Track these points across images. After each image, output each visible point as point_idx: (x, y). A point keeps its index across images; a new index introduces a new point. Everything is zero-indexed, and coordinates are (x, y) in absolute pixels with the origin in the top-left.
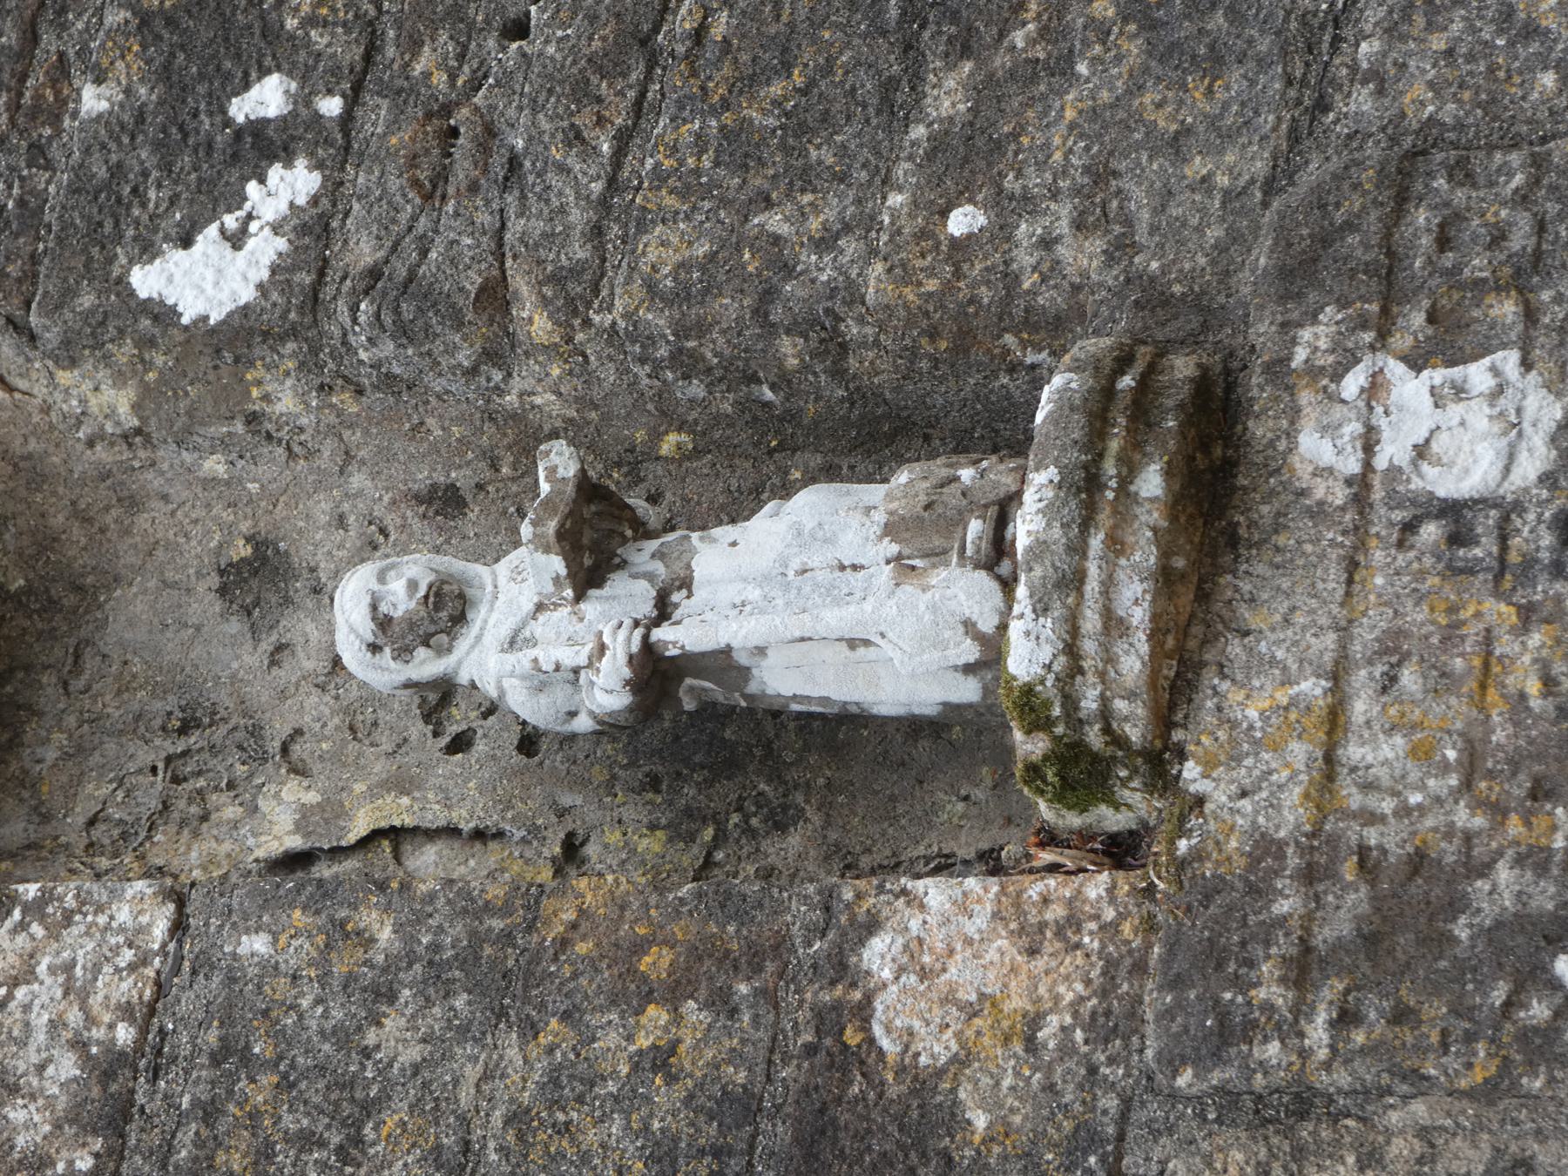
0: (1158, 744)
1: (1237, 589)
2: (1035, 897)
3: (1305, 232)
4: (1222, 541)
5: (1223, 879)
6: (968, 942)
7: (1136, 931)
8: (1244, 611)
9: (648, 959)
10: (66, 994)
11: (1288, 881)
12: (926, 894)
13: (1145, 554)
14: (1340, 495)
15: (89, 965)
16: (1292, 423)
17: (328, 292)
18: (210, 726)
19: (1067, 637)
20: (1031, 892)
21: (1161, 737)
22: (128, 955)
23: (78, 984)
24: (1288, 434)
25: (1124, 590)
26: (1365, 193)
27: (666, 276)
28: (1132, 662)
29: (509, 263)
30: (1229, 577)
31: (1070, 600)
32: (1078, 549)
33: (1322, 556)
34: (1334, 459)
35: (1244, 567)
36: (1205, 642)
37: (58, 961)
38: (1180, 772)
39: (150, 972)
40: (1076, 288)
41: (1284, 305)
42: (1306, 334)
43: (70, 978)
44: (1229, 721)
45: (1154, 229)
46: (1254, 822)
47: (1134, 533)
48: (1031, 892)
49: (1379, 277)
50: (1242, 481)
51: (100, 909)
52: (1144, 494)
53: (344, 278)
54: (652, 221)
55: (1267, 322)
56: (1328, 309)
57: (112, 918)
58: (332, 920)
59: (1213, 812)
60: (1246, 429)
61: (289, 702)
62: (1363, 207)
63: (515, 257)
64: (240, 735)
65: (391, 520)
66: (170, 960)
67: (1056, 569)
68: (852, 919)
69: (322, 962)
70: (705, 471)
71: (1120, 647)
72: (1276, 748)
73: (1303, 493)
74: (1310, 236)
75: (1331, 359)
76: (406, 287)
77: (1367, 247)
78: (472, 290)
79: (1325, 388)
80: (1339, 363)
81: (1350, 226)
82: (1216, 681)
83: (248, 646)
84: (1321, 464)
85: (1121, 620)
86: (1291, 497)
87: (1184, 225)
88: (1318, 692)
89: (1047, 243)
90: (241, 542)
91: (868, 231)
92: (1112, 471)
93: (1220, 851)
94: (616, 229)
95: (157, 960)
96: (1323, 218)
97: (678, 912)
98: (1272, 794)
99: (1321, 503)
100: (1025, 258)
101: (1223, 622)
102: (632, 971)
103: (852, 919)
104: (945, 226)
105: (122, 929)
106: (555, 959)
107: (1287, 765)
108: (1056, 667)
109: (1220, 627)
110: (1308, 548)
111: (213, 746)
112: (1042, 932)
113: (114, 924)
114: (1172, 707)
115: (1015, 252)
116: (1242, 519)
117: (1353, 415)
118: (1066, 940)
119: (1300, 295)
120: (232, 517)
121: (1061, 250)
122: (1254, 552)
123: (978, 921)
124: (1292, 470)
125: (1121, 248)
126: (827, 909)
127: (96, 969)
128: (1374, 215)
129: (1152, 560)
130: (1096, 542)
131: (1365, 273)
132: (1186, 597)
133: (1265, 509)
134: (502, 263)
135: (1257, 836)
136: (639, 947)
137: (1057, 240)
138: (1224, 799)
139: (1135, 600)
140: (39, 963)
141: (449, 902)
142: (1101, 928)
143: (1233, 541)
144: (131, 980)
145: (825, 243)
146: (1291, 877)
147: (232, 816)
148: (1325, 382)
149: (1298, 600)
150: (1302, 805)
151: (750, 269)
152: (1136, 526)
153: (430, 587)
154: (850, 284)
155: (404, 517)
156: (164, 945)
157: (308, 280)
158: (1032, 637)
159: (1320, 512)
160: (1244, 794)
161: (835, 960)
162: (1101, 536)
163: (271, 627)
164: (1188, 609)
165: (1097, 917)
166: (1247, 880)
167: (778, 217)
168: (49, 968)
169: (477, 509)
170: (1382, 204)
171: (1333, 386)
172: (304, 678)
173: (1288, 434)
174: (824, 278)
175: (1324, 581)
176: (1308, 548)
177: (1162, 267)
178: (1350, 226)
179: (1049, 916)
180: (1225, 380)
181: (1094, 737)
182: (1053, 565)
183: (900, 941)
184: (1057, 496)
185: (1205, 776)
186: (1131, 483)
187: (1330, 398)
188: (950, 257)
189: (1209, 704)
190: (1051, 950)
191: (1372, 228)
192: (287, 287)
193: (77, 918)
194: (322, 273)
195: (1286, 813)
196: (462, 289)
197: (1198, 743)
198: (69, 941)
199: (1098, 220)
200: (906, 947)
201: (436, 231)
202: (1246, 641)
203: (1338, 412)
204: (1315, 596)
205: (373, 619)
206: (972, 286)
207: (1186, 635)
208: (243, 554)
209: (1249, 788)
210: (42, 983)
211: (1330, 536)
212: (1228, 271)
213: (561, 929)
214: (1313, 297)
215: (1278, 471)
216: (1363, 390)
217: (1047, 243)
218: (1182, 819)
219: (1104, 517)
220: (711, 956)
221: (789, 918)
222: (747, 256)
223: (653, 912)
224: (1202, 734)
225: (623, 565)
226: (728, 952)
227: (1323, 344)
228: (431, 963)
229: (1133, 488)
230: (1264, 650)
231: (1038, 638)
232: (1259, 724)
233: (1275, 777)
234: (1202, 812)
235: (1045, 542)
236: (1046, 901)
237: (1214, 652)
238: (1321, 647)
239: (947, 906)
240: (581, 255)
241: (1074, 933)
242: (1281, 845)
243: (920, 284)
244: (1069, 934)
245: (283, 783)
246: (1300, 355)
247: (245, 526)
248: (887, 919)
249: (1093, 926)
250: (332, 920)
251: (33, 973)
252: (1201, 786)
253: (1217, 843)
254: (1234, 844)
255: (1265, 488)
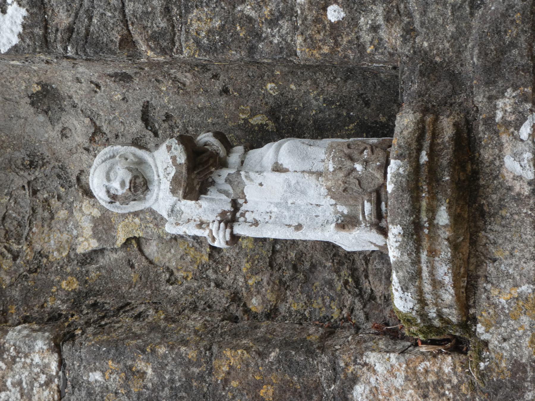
0: (464, 319)
1: (487, 238)
2: (422, 370)
3: (493, 48)
4: (477, 214)
5: (502, 382)
6: (397, 390)
7: (467, 389)
8: (491, 248)
9: (262, 391)
10: (22, 396)
11: (529, 384)
12: (375, 365)
13: (445, 252)
14: (526, 189)
15: (28, 382)
16: (500, 151)
17: (52, 37)
18: (43, 166)
19: (419, 298)
20: (420, 368)
21: (465, 315)
22: (43, 378)
23: (26, 391)
24: (499, 157)
25: (439, 270)
26: (517, 26)
27: (204, 37)
28: (448, 296)
29: (131, 27)
30: (483, 232)
31: (417, 284)
32: (417, 262)
33: (523, 222)
34: (521, 171)
35: (489, 227)
36: (477, 266)
37: (15, 381)
38: (476, 329)
39: (54, 386)
40: (391, 55)
41: (488, 87)
42: (500, 103)
43: (22, 389)
44: (493, 304)
45: (422, 24)
46: (511, 355)
47: (439, 245)
48: (420, 368)
49: (529, 72)
50: (482, 182)
51: (26, 356)
52: (441, 223)
53: (57, 30)
54: (192, 7)
55: (482, 96)
56: (508, 90)
57: (32, 360)
58: (126, 366)
59: (493, 349)
60: (480, 155)
61: (75, 156)
62: (518, 33)
63: (133, 24)
64: (57, 170)
65: (101, 82)
66: (61, 380)
67: (408, 273)
68: (346, 376)
69: (126, 386)
70: (237, 68)
71: (442, 292)
72: (516, 318)
73: (510, 189)
74: (495, 49)
75: (513, 117)
76: (86, 39)
77: (522, 57)
78: (117, 41)
79: (513, 133)
80: (518, 119)
81: (513, 45)
82: (485, 285)
83: (50, 127)
84: (516, 174)
85: (440, 282)
86: (505, 191)
87: (436, 23)
88: (530, 291)
89: (375, 28)
90: (35, 86)
91: (291, 17)
92: (425, 219)
93: (498, 367)
94: (175, 10)
95: (56, 380)
96: (500, 40)
97: (272, 369)
98: (517, 340)
99: (519, 194)
100: (366, 37)
101: (484, 256)
102: (257, 396)
103: (346, 376)
104: (326, 15)
105: (38, 365)
106: (224, 389)
107: (522, 327)
108: (415, 308)
109: (483, 258)
110: (516, 217)
111: (47, 176)
112: (428, 388)
113: (34, 363)
114: (468, 298)
115: (361, 34)
116: (484, 202)
117: (527, 149)
118: (438, 392)
119: (495, 82)
120: (28, 76)
121: (382, 33)
122: (492, 219)
123: (400, 380)
124: (503, 177)
125: (409, 32)
126: (334, 369)
127: (31, 384)
128: (523, 38)
129: (449, 254)
130: (424, 256)
131: (523, 71)
132: (465, 248)
133: (494, 197)
134: (127, 26)
135: (513, 361)
136: (258, 386)
137: (379, 27)
138: (496, 342)
139: (444, 272)
140: (6, 381)
141: (173, 359)
142: (452, 387)
143: (483, 214)
144: (47, 391)
145: (273, 22)
146: (530, 382)
147: (63, 216)
148: (512, 130)
149: (516, 244)
150: (530, 346)
151: (241, 35)
152: (440, 241)
153: (130, 183)
154: (288, 45)
155: (105, 82)
156: (57, 373)
157: (41, 33)
158: (404, 299)
159: (518, 199)
160: (505, 340)
161: (342, 396)
162: (425, 253)
163: (58, 120)
164: (468, 251)
165: (450, 381)
166: (512, 383)
167: (249, 7)
168: (12, 384)
169: (137, 79)
170: (526, 31)
171: (516, 132)
172: (79, 145)
173: (499, 157)
174: (276, 41)
175: (525, 234)
176: (516, 217)
177: (429, 46)
178: (513, 45)
179: (429, 380)
180: (467, 128)
181: (437, 323)
182: (407, 271)
183: (368, 388)
184: (403, 240)
185: (487, 332)
186: (434, 219)
187: (515, 138)
188: (331, 34)
189: (483, 296)
190: (433, 396)
191: (524, 46)
192: (32, 36)
193: (18, 359)
194: (46, 28)
195: (524, 350)
196: (112, 41)
197: (481, 315)
198: (17, 370)
199: (396, 15)
200: (371, 391)
201: (93, 7)
202: (495, 264)
203: (520, 146)
204: (523, 242)
205: (109, 196)
206: (344, 50)
207: (468, 263)
208: (37, 89)
209: (506, 337)
210: (10, 391)
211: (525, 211)
212: (459, 51)
213: (224, 375)
214: (500, 83)
215: (497, 176)
216: (530, 135)
217: (375, 28)
218: (480, 353)
219: (425, 243)
220: (289, 390)
221: (319, 375)
222: (238, 28)
223: (260, 368)
224: (483, 312)
225: (213, 183)
226: (296, 390)
227: (509, 109)
228: (171, 388)
229: (435, 222)
230: (504, 269)
231: (406, 300)
232: (506, 306)
233: (517, 332)
234: (488, 349)
235: (402, 261)
236: (427, 371)
237: (482, 270)
238: (528, 268)
239: (385, 372)
240: (162, 25)
241: (441, 388)
242: (524, 366)
243: (320, 48)
244: (439, 389)
245: (81, 202)
246: (499, 115)
247: (35, 79)
248: (361, 376)
249: (448, 386)
250: (126, 366)
251: (5, 386)
252: (485, 337)
253: (497, 364)
254: (503, 365)
255: (492, 186)
